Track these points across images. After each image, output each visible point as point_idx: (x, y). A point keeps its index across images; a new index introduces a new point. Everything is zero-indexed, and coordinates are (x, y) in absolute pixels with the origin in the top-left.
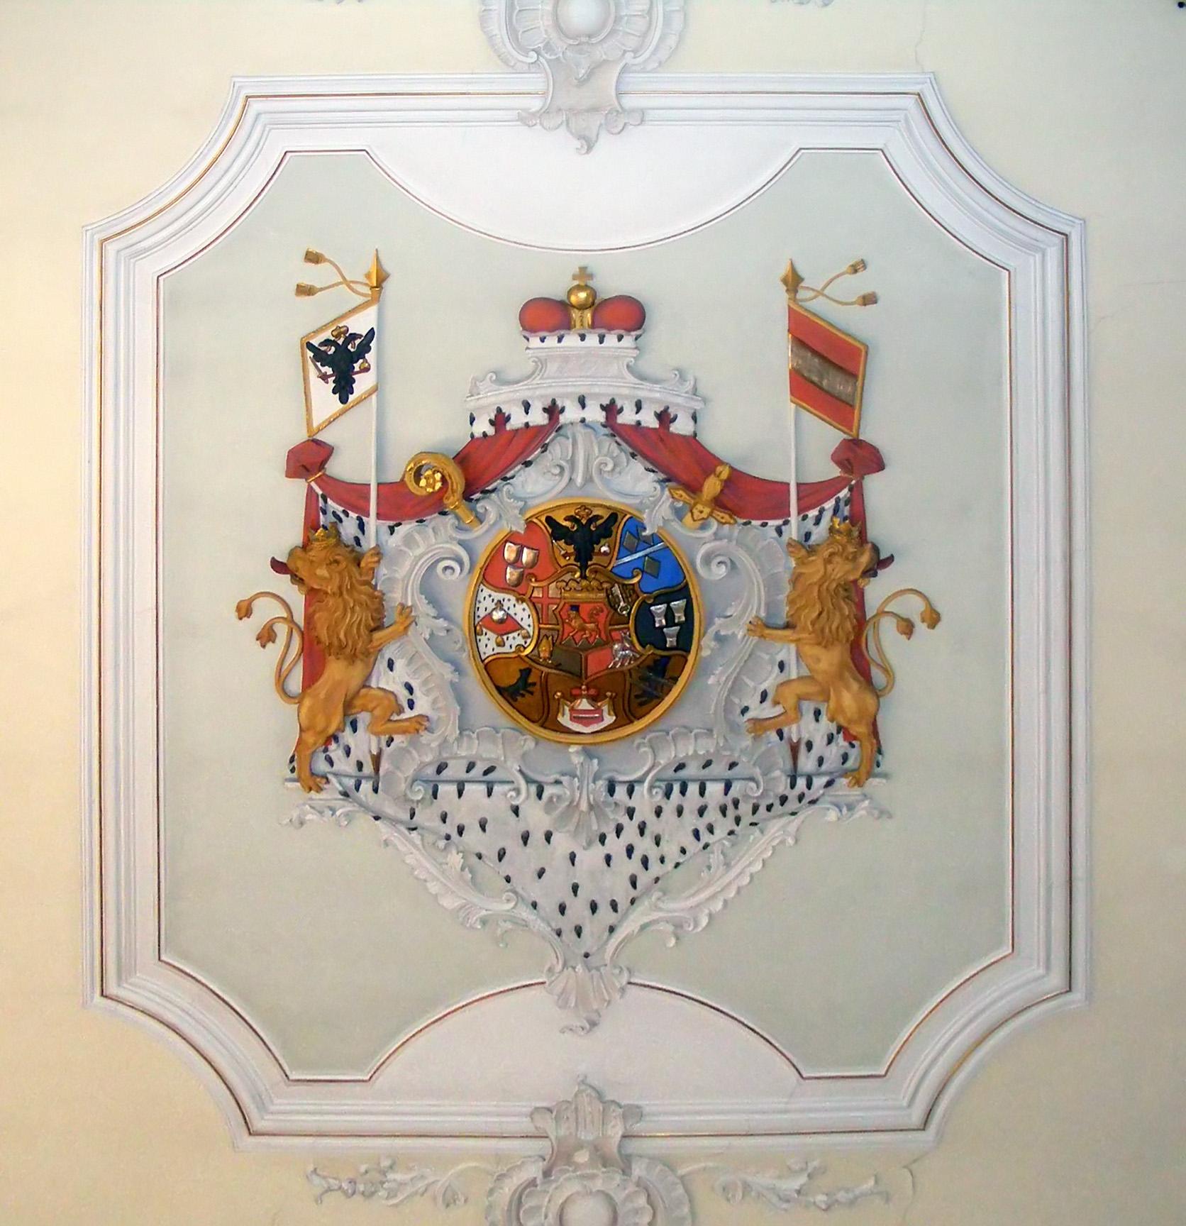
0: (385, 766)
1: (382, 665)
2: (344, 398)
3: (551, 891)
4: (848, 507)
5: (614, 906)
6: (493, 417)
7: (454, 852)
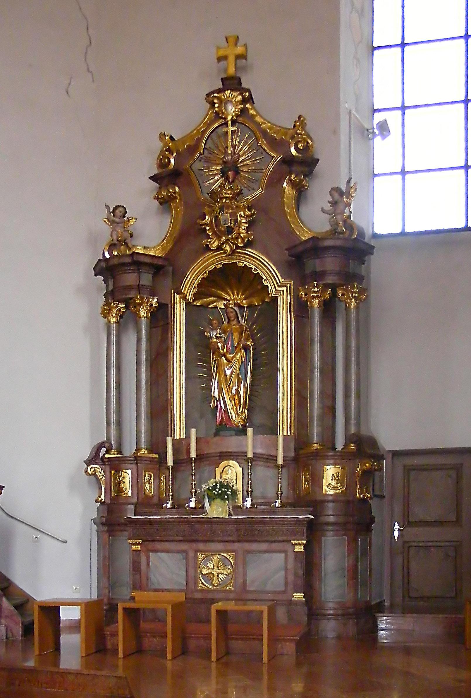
2: (152, 178)
4: (135, 451)
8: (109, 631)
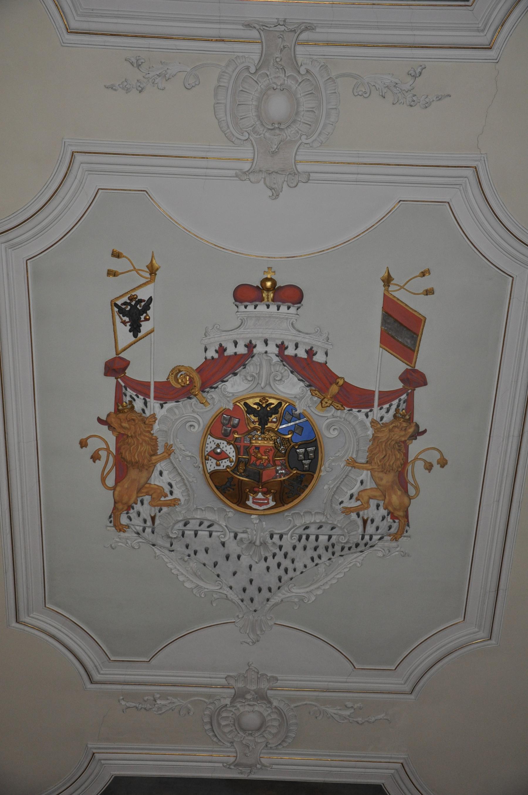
5: (270, 590)
6: (217, 348)
8: (387, 541)
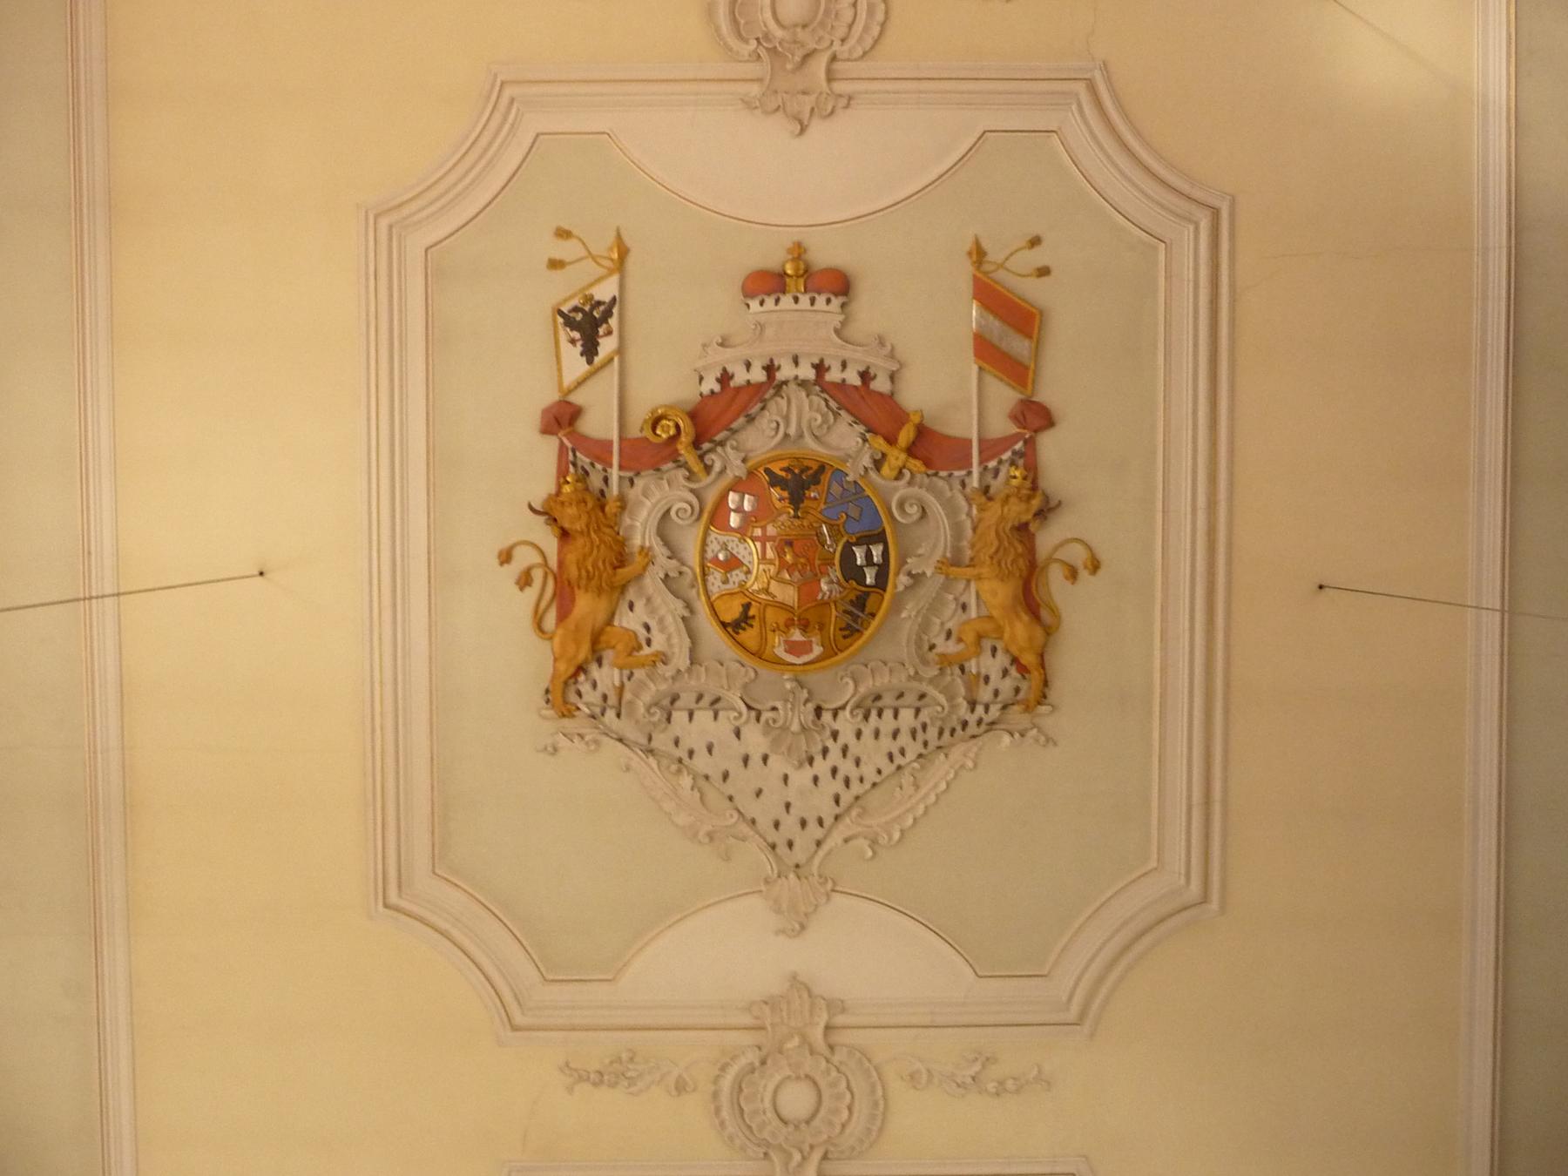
0: (627, 696)
1: (624, 606)
3: (764, 811)
5: (820, 822)
6: (719, 375)
7: (685, 773)
